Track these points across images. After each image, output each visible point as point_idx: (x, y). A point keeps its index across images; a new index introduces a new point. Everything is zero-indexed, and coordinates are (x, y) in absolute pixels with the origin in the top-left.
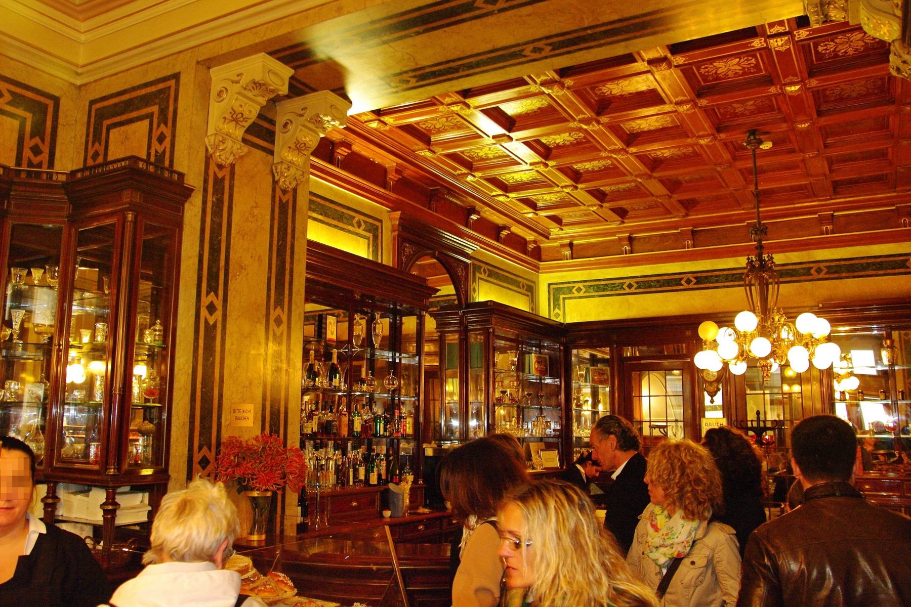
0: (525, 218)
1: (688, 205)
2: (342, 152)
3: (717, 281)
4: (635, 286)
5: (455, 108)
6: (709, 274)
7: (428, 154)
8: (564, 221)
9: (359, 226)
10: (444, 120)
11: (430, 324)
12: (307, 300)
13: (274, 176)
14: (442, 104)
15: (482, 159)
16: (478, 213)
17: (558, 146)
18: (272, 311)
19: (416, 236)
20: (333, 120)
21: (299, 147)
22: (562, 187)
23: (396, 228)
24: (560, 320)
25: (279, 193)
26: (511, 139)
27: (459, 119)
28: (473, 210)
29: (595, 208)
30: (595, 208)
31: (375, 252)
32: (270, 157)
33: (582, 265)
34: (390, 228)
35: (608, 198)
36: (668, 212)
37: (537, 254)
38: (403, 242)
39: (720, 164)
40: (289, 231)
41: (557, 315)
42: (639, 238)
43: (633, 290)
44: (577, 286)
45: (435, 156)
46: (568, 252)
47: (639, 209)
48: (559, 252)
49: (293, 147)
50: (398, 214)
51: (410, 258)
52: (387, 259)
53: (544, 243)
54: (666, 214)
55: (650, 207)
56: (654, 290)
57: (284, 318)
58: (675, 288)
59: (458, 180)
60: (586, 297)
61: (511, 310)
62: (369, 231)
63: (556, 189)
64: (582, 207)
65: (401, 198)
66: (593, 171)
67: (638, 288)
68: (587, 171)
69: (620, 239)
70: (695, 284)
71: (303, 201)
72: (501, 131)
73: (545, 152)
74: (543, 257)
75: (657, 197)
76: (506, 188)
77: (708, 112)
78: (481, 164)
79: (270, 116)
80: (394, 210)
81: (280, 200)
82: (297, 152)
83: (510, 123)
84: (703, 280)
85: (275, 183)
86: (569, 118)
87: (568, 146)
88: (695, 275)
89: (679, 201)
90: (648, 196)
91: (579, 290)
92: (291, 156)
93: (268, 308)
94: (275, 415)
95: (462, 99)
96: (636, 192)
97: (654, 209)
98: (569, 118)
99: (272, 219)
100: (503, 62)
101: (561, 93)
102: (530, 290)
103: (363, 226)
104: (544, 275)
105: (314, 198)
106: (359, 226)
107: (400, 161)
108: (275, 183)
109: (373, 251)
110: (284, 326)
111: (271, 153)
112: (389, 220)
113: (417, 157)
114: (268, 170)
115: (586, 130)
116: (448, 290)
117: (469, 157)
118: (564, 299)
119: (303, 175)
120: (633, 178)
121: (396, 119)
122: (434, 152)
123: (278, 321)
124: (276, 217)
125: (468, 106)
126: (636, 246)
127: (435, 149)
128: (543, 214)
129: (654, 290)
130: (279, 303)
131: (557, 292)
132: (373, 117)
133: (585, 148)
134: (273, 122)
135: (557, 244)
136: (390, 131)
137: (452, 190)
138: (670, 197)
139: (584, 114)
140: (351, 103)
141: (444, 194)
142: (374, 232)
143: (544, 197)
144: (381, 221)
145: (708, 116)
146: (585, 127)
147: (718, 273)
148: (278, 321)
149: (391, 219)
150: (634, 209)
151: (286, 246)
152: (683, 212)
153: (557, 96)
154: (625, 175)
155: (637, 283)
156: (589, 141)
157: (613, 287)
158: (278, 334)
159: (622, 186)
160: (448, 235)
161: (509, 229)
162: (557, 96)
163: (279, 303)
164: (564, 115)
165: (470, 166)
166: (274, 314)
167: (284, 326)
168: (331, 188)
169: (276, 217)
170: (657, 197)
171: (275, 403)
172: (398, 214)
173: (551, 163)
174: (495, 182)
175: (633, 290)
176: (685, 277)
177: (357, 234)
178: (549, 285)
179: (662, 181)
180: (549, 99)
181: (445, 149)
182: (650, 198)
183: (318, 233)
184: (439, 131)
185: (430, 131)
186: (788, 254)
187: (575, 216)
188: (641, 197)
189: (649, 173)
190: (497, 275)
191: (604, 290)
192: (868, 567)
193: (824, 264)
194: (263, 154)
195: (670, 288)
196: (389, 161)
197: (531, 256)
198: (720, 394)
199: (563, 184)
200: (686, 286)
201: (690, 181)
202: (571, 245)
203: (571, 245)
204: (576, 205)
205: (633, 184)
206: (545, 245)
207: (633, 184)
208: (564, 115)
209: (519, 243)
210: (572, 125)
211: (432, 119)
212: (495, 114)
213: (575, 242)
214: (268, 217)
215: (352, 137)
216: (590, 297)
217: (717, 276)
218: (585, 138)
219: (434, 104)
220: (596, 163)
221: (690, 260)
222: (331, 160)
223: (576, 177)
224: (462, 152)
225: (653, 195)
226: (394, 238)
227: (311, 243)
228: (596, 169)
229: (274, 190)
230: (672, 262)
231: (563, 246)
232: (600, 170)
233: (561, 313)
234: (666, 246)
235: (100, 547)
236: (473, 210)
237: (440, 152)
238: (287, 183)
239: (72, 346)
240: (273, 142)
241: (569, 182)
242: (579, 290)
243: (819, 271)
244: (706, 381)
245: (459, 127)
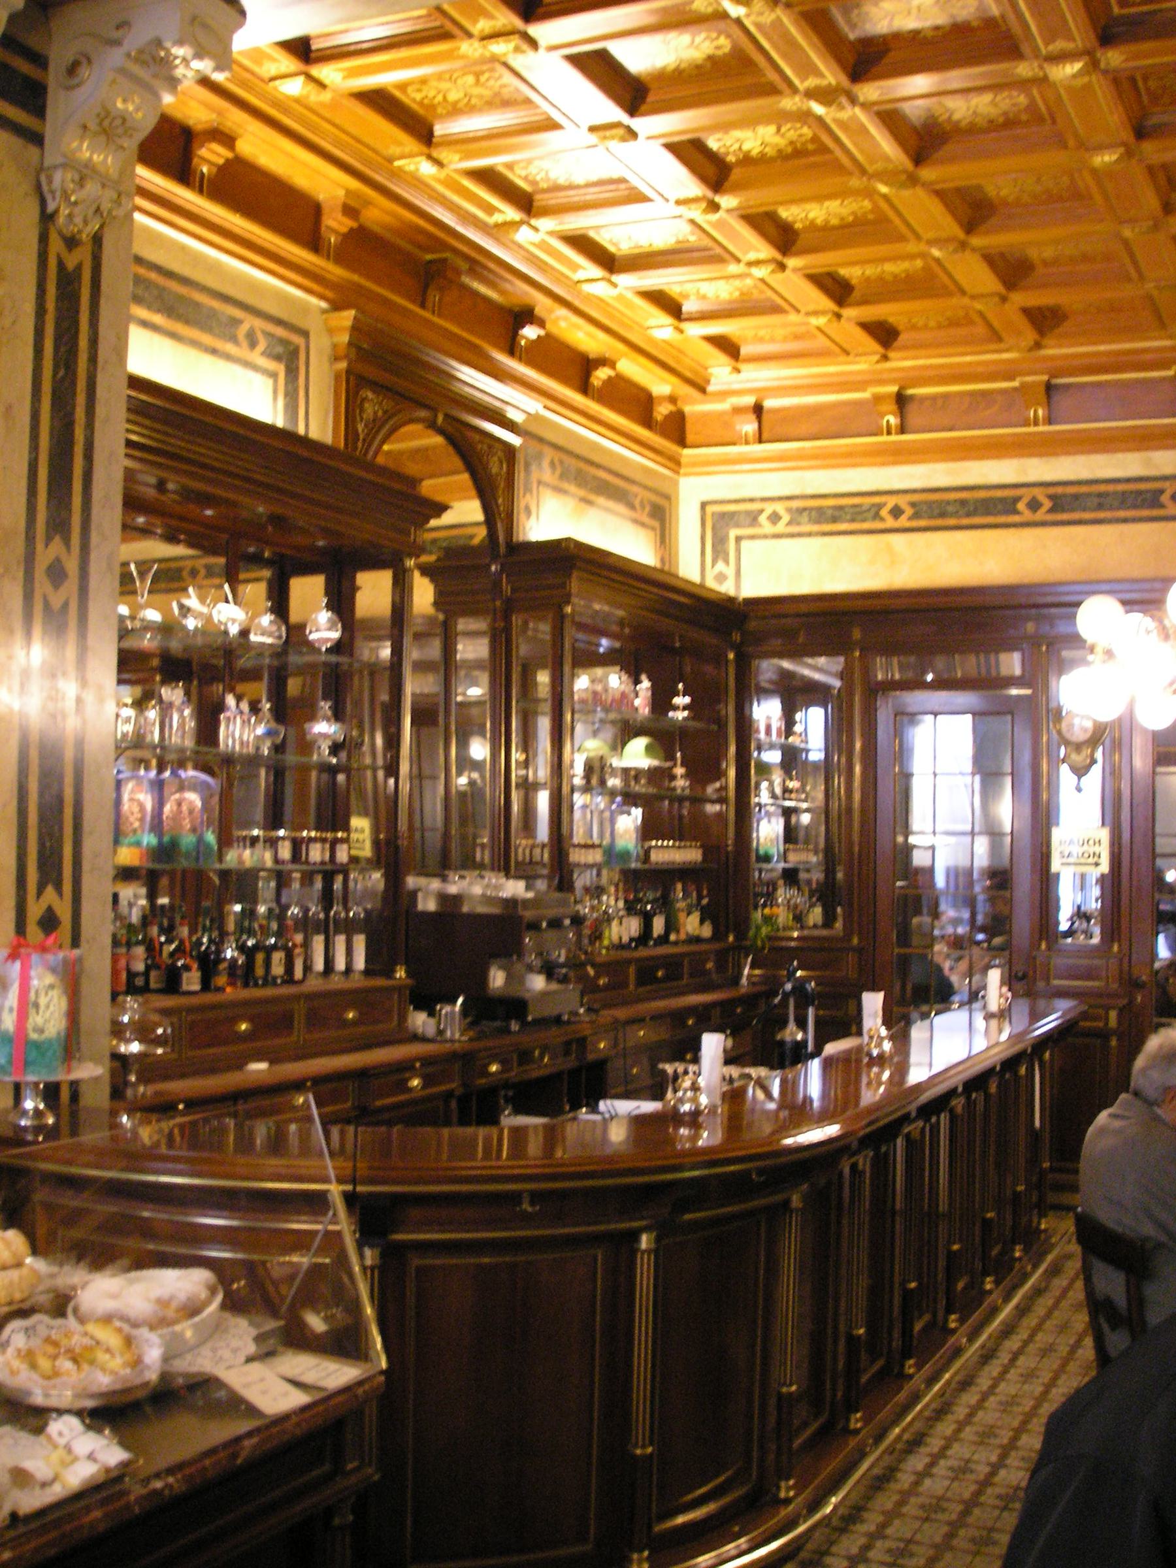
0: (651, 340)
1: (1044, 321)
2: (210, 156)
3: (1100, 507)
4: (909, 512)
5: (500, 48)
6: (1084, 489)
7: (426, 169)
8: (744, 351)
9: (253, 344)
10: (470, 79)
11: (423, 594)
12: (129, 530)
13: (43, 203)
14: (469, 35)
15: (556, 188)
16: (541, 323)
17: (747, 160)
18: (40, 546)
19: (387, 375)
20: (199, 56)
21: (108, 127)
22: (750, 264)
23: (342, 351)
24: (727, 588)
25: (56, 245)
26: (632, 134)
27: (508, 78)
28: (526, 315)
29: (821, 321)
30: (821, 321)
31: (291, 408)
32: (33, 151)
33: (781, 458)
34: (328, 350)
35: (856, 294)
36: (995, 336)
37: (677, 429)
38: (358, 387)
39: (1132, 221)
40: (83, 343)
41: (721, 577)
42: (923, 399)
43: (903, 521)
44: (769, 508)
45: (443, 174)
46: (749, 427)
47: (926, 327)
48: (728, 425)
49: (93, 125)
50: (347, 317)
51: (375, 426)
52: (319, 424)
53: (694, 402)
54: (990, 341)
55: (953, 323)
56: (952, 522)
57: (72, 565)
58: (1002, 519)
59: (497, 240)
60: (792, 535)
61: (610, 561)
62: (278, 358)
63: (733, 268)
64: (792, 317)
65: (355, 278)
66: (826, 228)
67: (916, 516)
68: (812, 226)
69: (877, 399)
70: (1050, 511)
71: (116, 277)
72: (613, 112)
73: (711, 169)
74: (690, 437)
75: (973, 297)
76: (609, 262)
77: (1125, 85)
78: (553, 200)
79: (33, 41)
80: (337, 306)
81: (61, 265)
82: (103, 138)
83: (633, 93)
84: (1066, 504)
85: (47, 218)
86: (781, 85)
87: (772, 160)
88: (1052, 491)
89: (1026, 311)
90: (950, 294)
91: (775, 518)
92: (86, 151)
93: (30, 538)
94: (51, 813)
95: (518, 23)
96: (924, 285)
97: (963, 328)
98: (781, 85)
99: (40, 311)
101: (768, 17)
102: (659, 516)
103: (262, 345)
104: (692, 479)
105: (142, 271)
106: (253, 344)
107: (354, 184)
108: (47, 218)
109: (286, 407)
110: (71, 585)
111: (37, 139)
112: (329, 331)
113: (397, 174)
114: (26, 187)
115: (820, 120)
116: (466, 512)
117: (526, 179)
118: (738, 539)
119: (118, 202)
120: (922, 247)
121: (352, 73)
122: (439, 163)
123: (57, 574)
124: (51, 305)
125: (533, 44)
126: (915, 416)
127: (443, 154)
128: (695, 330)
129: (952, 522)
130: (59, 526)
131: (722, 524)
132: (287, 63)
133: (814, 166)
134: (40, 60)
135: (725, 406)
136: (334, 105)
137: (479, 262)
138: (1004, 299)
139: (822, 76)
140: (243, 13)
141: (459, 273)
142: (290, 360)
143: (694, 286)
144: (305, 334)
145: (1120, 96)
146: (818, 109)
147: (1102, 488)
148: (57, 574)
149: (331, 331)
150: (914, 327)
151: (73, 383)
152: (1030, 336)
153: (759, 26)
154: (902, 238)
155: (913, 505)
156: (823, 149)
157: (857, 514)
158: (56, 601)
159: (890, 268)
160: (467, 374)
161: (611, 364)
162: (759, 26)
163: (59, 526)
164: (772, 76)
165: (526, 203)
166: (45, 555)
167: (71, 585)
168: (183, 248)
169: (51, 305)
170: (973, 297)
171: (50, 775)
172: (347, 317)
173: (727, 201)
174: (583, 244)
175: (903, 521)
176: (1027, 494)
177: (247, 364)
178: (704, 505)
179: (991, 260)
180: (737, 32)
181: (469, 156)
182: (955, 301)
183: (156, 356)
184: (456, 111)
185: (432, 107)
187: (772, 340)
188: (937, 296)
189: (961, 235)
190: (594, 480)
191: (834, 520)
194: (16, 142)
195: (990, 520)
196: (323, 182)
197: (664, 434)
198: (1096, 771)
199: (752, 256)
200: (1027, 515)
201: (1055, 262)
202: (758, 409)
203: (758, 409)
204: (775, 310)
205: (919, 263)
206: (695, 407)
207: (919, 263)
208: (772, 76)
209: (637, 404)
210: (789, 103)
211: (439, 77)
212: (598, 66)
213: (768, 404)
214: (29, 307)
215: (235, 118)
216: (800, 535)
217: (1100, 495)
218: (815, 139)
219: (445, 36)
220: (834, 206)
221: (1040, 455)
222: (183, 173)
223: (784, 238)
224: (510, 166)
225: (963, 292)
226: (337, 377)
227: (136, 383)
228: (834, 221)
229: (44, 239)
230: (998, 456)
231: (738, 411)
232: (844, 226)
233: (730, 571)
234: (973, 418)
236: (526, 315)
237: (456, 162)
238: (78, 220)
240: (40, 112)
241: (764, 251)
242: (775, 518)
244: (1067, 743)
245: (505, 103)
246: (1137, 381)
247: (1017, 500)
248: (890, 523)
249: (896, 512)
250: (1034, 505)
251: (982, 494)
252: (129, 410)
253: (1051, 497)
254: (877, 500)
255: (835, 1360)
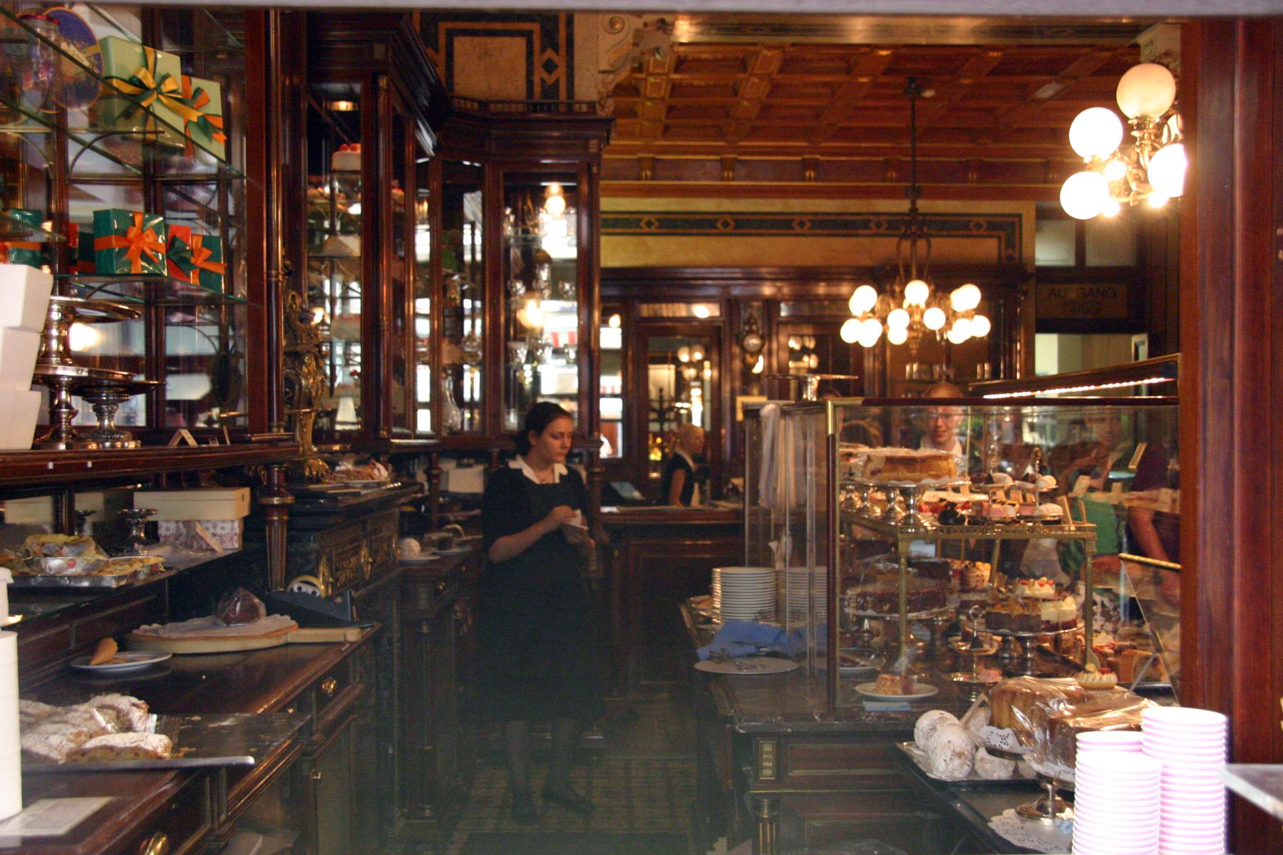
3: (760, 227)
43: (653, 229)
67: (660, 227)
100: (1246, 229)
118: (999, 238)
175: (653, 229)
186: (847, 201)
191: (614, 227)
192: (1210, 435)
193: (886, 217)
221: (728, 197)
235: (908, 368)
239: (914, 243)
243: (879, 225)
246: (785, 162)
247: (716, 220)
248: (646, 230)
249: (649, 224)
250: (726, 224)
251: (698, 217)
252: (1068, 795)
253: (735, 221)
254: (638, 216)
255: (787, 470)
